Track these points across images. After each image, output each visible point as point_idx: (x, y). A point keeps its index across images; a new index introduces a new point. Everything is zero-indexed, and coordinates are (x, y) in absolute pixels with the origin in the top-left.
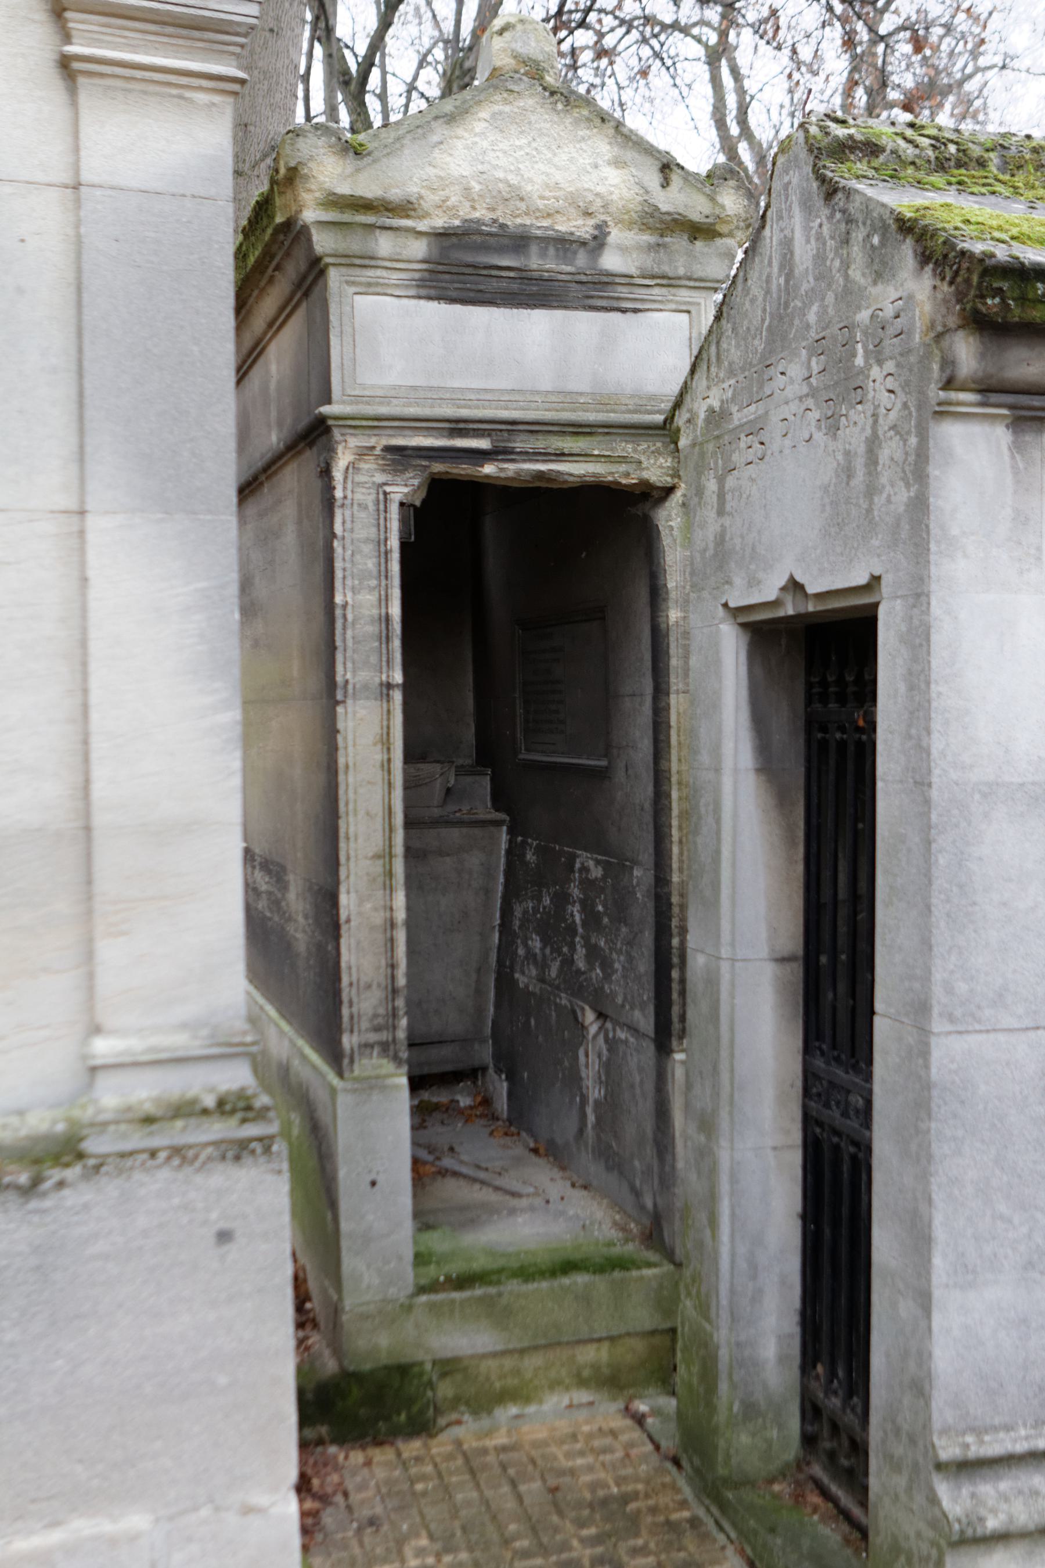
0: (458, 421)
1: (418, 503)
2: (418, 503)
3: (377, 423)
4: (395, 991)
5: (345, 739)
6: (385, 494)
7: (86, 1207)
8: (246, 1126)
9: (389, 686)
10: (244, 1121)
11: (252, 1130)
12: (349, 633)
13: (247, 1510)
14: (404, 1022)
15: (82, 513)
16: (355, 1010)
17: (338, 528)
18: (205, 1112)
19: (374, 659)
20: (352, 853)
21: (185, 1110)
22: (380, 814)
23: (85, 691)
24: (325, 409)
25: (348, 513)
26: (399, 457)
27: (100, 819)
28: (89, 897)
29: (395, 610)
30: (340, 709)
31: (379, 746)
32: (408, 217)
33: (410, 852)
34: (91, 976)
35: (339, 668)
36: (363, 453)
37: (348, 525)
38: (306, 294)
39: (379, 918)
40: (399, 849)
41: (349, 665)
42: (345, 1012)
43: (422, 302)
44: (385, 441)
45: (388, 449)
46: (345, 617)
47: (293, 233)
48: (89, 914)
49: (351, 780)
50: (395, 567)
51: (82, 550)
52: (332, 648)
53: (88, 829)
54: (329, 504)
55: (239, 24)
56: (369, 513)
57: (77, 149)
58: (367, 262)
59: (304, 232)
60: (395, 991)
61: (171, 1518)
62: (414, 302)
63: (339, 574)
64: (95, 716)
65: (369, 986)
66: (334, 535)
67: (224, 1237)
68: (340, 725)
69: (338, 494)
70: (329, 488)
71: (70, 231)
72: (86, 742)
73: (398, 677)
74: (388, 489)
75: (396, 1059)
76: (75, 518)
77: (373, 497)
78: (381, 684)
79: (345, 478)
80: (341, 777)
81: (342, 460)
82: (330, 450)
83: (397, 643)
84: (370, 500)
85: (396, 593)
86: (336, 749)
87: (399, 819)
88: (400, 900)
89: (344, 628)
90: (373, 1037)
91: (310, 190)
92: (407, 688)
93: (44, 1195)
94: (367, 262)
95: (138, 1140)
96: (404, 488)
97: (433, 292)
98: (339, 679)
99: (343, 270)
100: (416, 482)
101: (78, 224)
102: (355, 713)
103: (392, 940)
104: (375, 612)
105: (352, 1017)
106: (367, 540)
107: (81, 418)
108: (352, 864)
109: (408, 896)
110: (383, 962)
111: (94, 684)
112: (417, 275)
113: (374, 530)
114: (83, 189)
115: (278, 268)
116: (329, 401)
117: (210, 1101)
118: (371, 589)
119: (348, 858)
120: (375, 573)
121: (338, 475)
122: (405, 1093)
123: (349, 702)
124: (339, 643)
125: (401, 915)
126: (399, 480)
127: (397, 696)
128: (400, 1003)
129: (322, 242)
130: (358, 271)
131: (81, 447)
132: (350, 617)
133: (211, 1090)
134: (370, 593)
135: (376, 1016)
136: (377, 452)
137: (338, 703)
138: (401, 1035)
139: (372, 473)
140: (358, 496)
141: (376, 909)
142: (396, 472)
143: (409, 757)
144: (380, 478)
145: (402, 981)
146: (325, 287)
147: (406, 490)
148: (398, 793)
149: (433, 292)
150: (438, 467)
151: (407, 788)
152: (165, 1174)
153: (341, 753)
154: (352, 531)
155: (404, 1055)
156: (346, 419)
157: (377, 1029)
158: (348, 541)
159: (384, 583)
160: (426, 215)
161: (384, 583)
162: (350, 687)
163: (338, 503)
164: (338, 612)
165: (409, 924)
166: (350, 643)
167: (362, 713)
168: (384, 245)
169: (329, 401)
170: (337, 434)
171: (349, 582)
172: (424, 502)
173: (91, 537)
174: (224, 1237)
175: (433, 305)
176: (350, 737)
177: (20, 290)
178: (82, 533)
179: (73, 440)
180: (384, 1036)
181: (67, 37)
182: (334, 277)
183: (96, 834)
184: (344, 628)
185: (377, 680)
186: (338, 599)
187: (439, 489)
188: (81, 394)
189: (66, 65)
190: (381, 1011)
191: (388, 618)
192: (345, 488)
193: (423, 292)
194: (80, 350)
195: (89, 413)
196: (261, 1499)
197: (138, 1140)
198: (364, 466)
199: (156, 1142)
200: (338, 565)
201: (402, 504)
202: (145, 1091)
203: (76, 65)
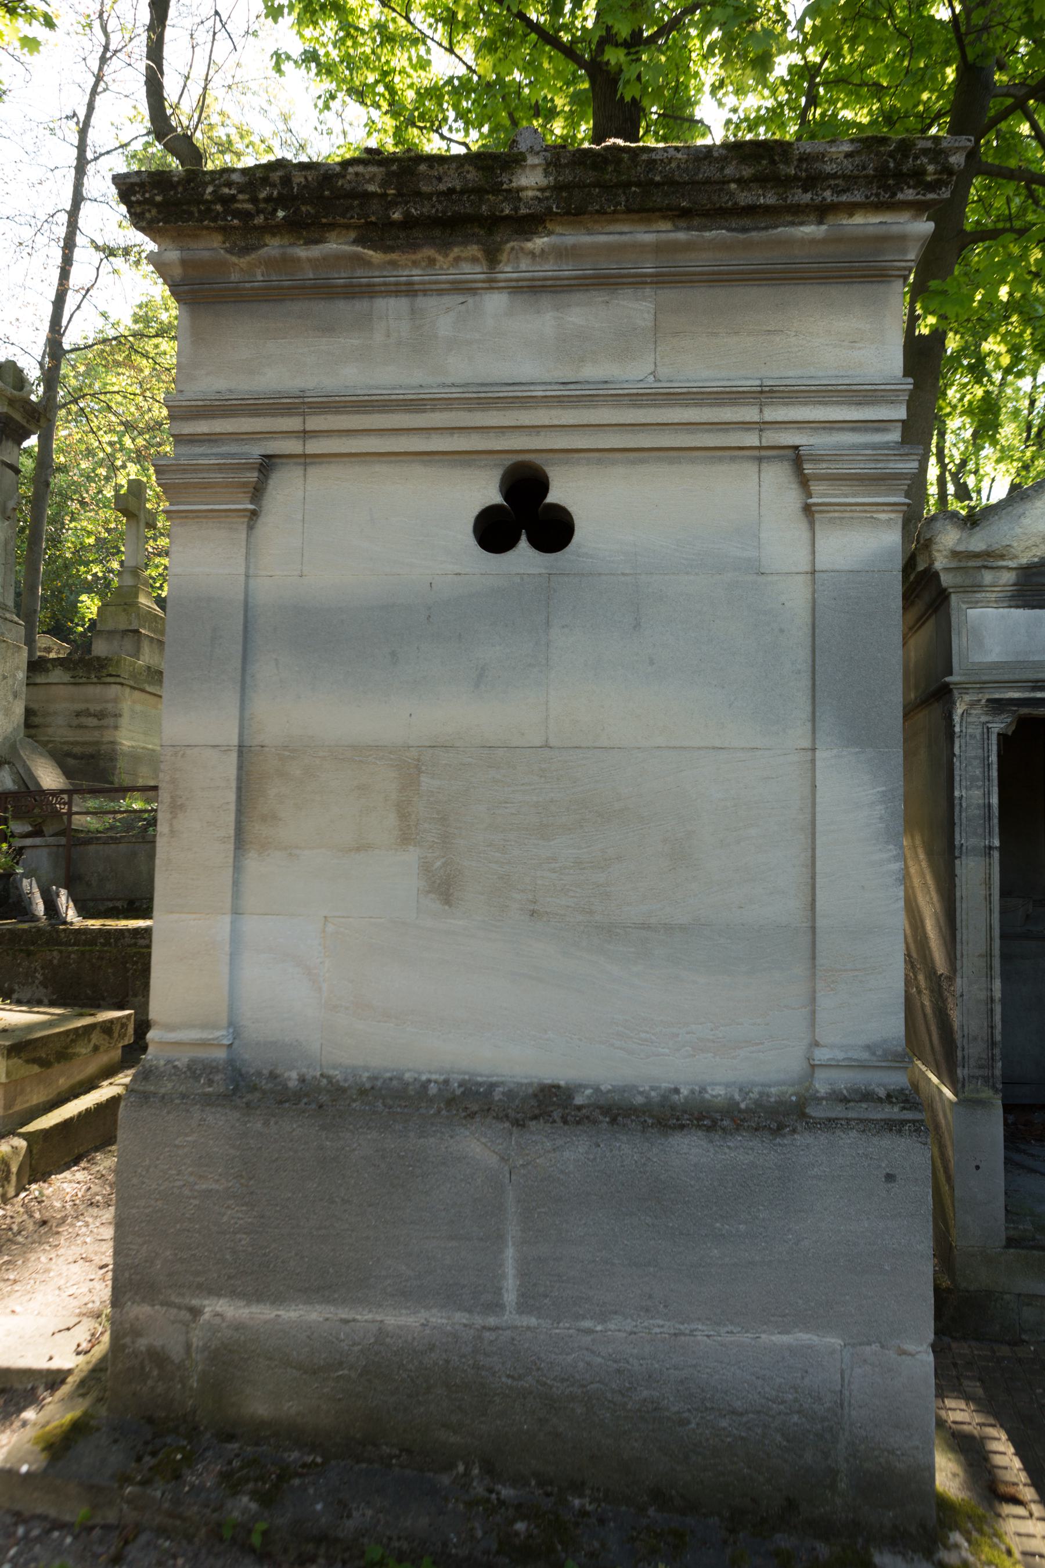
0: (1037, 681)
1: (1010, 733)
2: (1010, 733)
3: (983, 685)
4: (993, 1044)
5: (961, 881)
6: (988, 728)
7: (808, 1146)
8: (905, 1112)
9: (990, 848)
10: (904, 1108)
11: (908, 1115)
12: (964, 814)
13: (903, 1353)
14: (1000, 1064)
15: (814, 750)
16: (966, 1052)
17: (957, 751)
18: (880, 1100)
19: (980, 831)
20: (965, 953)
21: (867, 1096)
22: (984, 929)
23: (814, 849)
24: (948, 679)
25: (963, 741)
26: (997, 706)
27: (820, 923)
28: (814, 966)
29: (995, 800)
30: (957, 862)
31: (983, 886)
32: (1004, 560)
33: (1005, 957)
34: (813, 1012)
35: (957, 836)
36: (972, 704)
37: (963, 748)
38: (936, 610)
39: (983, 995)
40: (997, 952)
41: (964, 834)
42: (959, 1054)
43: (1012, 610)
44: (988, 696)
45: (988, 700)
46: (961, 804)
47: (931, 576)
48: (814, 974)
49: (964, 906)
50: (995, 774)
51: (814, 769)
52: (952, 824)
53: (813, 929)
54: (950, 736)
55: (907, 474)
56: (976, 736)
57: (814, 553)
58: (975, 589)
59: (936, 575)
60: (993, 1044)
61: (854, 1345)
62: (1006, 610)
63: (957, 778)
64: (818, 864)
65: (975, 1039)
66: (954, 755)
67: (890, 1178)
68: (958, 872)
69: (957, 729)
70: (950, 725)
71: (809, 596)
72: (813, 878)
73: (996, 843)
74: (990, 725)
75: (996, 1091)
76: (810, 753)
77: (979, 731)
78: (985, 847)
79: (962, 720)
80: (958, 904)
81: (960, 709)
82: (950, 705)
83: (996, 821)
84: (978, 732)
85: (995, 790)
86: (955, 886)
87: (997, 933)
88: (997, 984)
89: (960, 812)
90: (978, 1072)
91: (939, 551)
92: (1001, 849)
93: (784, 1136)
94: (975, 589)
95: (838, 1111)
96: (999, 725)
97: (1020, 603)
98: (957, 843)
99: (961, 595)
100: (1009, 720)
101: (814, 592)
102: (967, 864)
103: (992, 1010)
104: (981, 801)
105: (964, 1057)
106: (976, 758)
107: (814, 697)
108: (965, 960)
109: (1002, 982)
110: (985, 1024)
111: (818, 842)
112: (1009, 594)
113: (980, 751)
114: (817, 574)
115: (917, 596)
116: (951, 674)
117: (882, 1093)
118: (978, 788)
119: (962, 956)
120: (981, 776)
121: (957, 719)
122: (1000, 1111)
123: (964, 857)
124: (957, 820)
125: (998, 995)
126: (997, 719)
127: (996, 854)
128: (997, 1051)
129: (946, 580)
130: (970, 595)
131: (814, 713)
132: (964, 805)
133: (884, 1086)
134: (977, 790)
135: (980, 1058)
136: (983, 702)
137: (956, 858)
138: (998, 1072)
139: (979, 716)
140: (969, 731)
141: (981, 990)
142: (994, 715)
143: (1004, 894)
144: (984, 719)
145: (998, 1037)
146: (949, 606)
147: (1002, 725)
148: (996, 915)
149: (1020, 603)
150: (1024, 711)
151: (1001, 913)
152: (854, 1134)
153: (958, 889)
154: (966, 751)
155: (1000, 1086)
156: (774, 457)
157: (981, 1067)
158: (963, 758)
159: (987, 783)
160: (1016, 557)
161: (987, 783)
162: (964, 848)
163: (957, 735)
164: (957, 802)
165: (1003, 1001)
166: (964, 821)
167: (972, 864)
168: (988, 577)
169: (950, 673)
170: (955, 692)
171: (964, 783)
172: (1014, 732)
173: (819, 764)
174: (890, 1178)
175: (1020, 611)
176: (964, 880)
177: (782, 631)
178: (813, 761)
179: (809, 709)
180: (986, 1072)
181: (810, 495)
182: (954, 598)
183: (818, 931)
184: (960, 812)
185: (983, 844)
186: (957, 794)
187: (1023, 723)
188: (814, 685)
189: (808, 510)
190: (984, 1056)
191: (989, 805)
192: (961, 726)
193: (1012, 603)
194: (814, 661)
195: (818, 694)
196: (910, 1347)
197: (838, 1111)
198: (973, 712)
199: (851, 1115)
200: (957, 772)
201: (999, 734)
202: (844, 1080)
203: (814, 508)
